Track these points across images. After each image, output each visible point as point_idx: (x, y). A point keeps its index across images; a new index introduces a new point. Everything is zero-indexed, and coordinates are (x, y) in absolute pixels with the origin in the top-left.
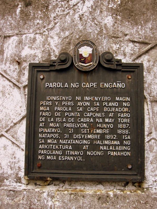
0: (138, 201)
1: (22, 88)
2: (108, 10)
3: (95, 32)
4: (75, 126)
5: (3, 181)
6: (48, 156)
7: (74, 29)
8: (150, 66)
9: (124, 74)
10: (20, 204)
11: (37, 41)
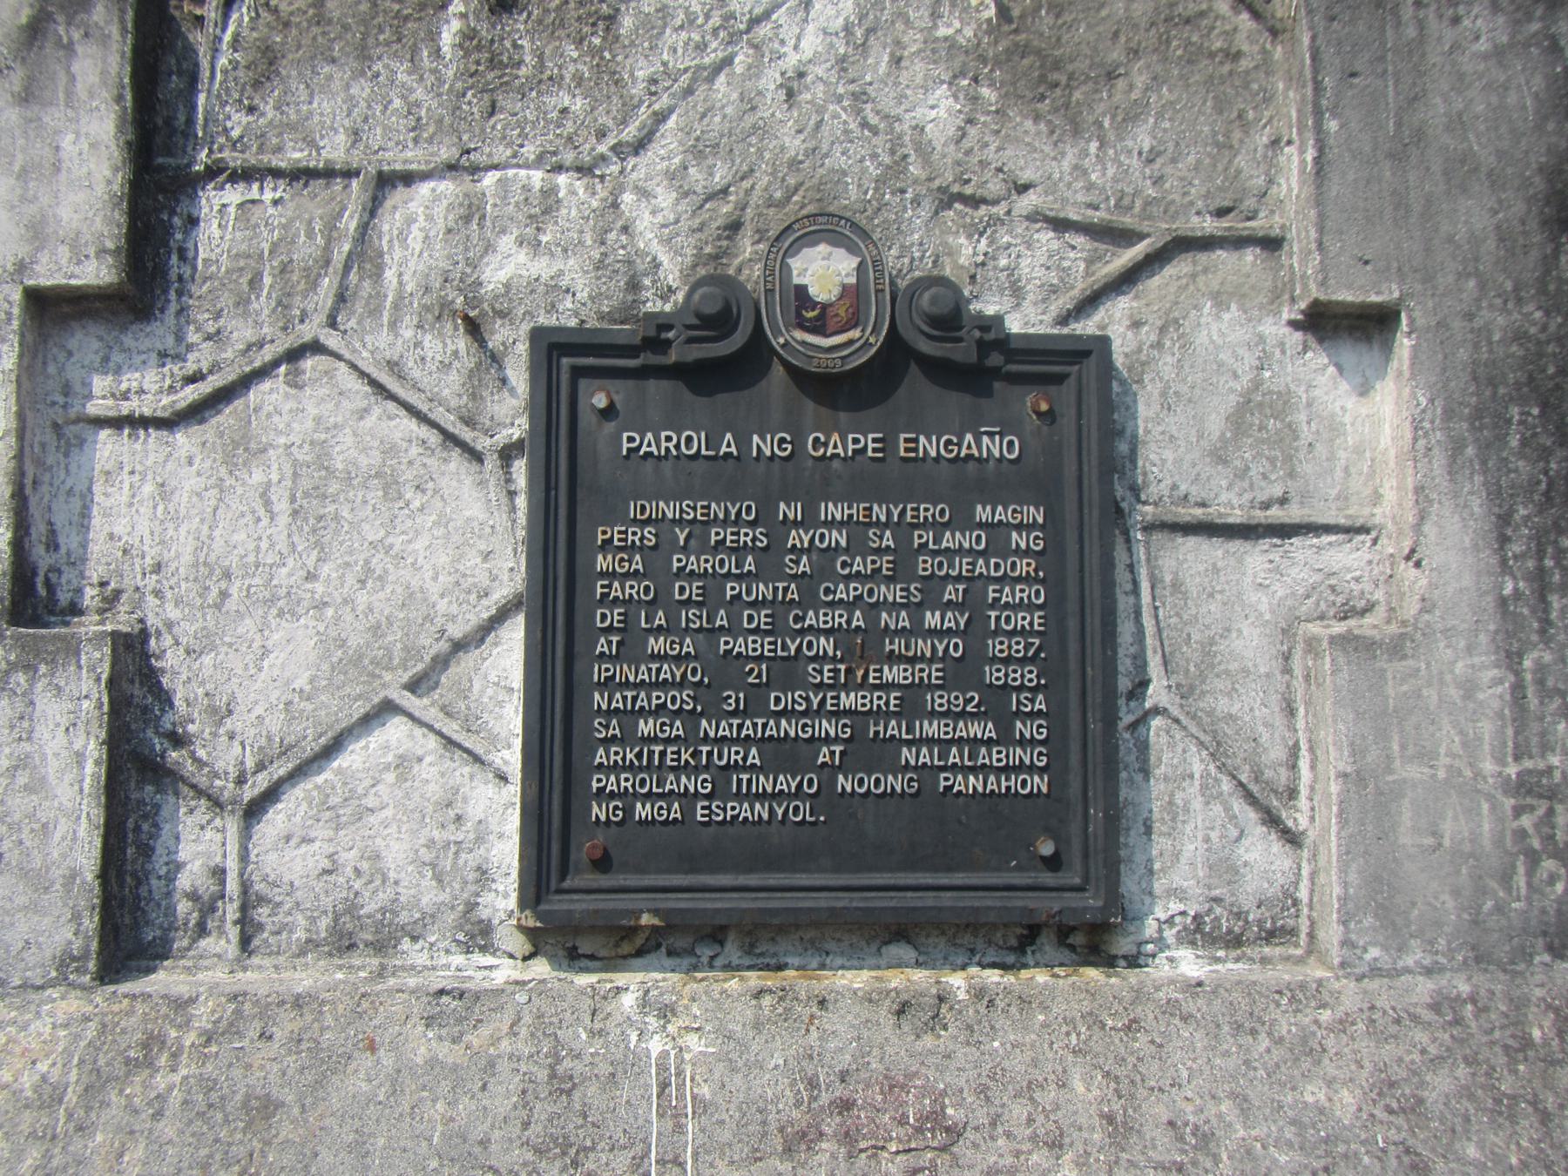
0: (1090, 1020)
1: (495, 456)
2: (934, 51)
3: (864, 171)
4: (775, 651)
5: (391, 951)
6: (639, 805)
7: (760, 152)
8: (1140, 350)
9: (1018, 389)
10: (499, 1056)
11: (564, 211)
